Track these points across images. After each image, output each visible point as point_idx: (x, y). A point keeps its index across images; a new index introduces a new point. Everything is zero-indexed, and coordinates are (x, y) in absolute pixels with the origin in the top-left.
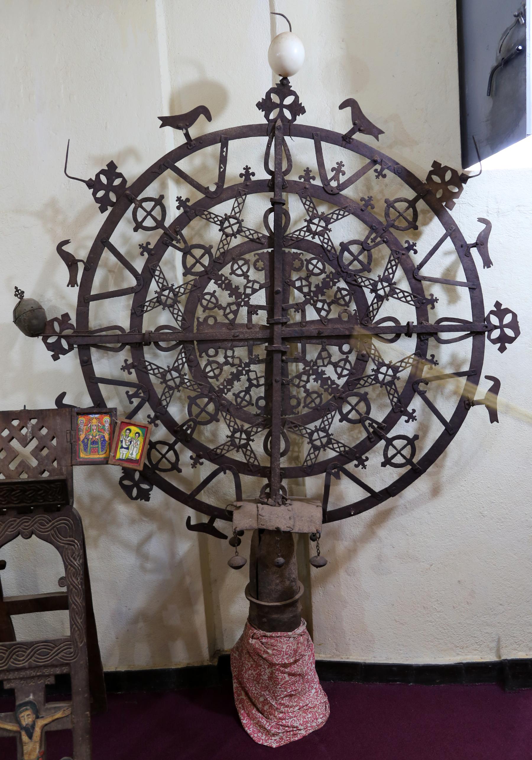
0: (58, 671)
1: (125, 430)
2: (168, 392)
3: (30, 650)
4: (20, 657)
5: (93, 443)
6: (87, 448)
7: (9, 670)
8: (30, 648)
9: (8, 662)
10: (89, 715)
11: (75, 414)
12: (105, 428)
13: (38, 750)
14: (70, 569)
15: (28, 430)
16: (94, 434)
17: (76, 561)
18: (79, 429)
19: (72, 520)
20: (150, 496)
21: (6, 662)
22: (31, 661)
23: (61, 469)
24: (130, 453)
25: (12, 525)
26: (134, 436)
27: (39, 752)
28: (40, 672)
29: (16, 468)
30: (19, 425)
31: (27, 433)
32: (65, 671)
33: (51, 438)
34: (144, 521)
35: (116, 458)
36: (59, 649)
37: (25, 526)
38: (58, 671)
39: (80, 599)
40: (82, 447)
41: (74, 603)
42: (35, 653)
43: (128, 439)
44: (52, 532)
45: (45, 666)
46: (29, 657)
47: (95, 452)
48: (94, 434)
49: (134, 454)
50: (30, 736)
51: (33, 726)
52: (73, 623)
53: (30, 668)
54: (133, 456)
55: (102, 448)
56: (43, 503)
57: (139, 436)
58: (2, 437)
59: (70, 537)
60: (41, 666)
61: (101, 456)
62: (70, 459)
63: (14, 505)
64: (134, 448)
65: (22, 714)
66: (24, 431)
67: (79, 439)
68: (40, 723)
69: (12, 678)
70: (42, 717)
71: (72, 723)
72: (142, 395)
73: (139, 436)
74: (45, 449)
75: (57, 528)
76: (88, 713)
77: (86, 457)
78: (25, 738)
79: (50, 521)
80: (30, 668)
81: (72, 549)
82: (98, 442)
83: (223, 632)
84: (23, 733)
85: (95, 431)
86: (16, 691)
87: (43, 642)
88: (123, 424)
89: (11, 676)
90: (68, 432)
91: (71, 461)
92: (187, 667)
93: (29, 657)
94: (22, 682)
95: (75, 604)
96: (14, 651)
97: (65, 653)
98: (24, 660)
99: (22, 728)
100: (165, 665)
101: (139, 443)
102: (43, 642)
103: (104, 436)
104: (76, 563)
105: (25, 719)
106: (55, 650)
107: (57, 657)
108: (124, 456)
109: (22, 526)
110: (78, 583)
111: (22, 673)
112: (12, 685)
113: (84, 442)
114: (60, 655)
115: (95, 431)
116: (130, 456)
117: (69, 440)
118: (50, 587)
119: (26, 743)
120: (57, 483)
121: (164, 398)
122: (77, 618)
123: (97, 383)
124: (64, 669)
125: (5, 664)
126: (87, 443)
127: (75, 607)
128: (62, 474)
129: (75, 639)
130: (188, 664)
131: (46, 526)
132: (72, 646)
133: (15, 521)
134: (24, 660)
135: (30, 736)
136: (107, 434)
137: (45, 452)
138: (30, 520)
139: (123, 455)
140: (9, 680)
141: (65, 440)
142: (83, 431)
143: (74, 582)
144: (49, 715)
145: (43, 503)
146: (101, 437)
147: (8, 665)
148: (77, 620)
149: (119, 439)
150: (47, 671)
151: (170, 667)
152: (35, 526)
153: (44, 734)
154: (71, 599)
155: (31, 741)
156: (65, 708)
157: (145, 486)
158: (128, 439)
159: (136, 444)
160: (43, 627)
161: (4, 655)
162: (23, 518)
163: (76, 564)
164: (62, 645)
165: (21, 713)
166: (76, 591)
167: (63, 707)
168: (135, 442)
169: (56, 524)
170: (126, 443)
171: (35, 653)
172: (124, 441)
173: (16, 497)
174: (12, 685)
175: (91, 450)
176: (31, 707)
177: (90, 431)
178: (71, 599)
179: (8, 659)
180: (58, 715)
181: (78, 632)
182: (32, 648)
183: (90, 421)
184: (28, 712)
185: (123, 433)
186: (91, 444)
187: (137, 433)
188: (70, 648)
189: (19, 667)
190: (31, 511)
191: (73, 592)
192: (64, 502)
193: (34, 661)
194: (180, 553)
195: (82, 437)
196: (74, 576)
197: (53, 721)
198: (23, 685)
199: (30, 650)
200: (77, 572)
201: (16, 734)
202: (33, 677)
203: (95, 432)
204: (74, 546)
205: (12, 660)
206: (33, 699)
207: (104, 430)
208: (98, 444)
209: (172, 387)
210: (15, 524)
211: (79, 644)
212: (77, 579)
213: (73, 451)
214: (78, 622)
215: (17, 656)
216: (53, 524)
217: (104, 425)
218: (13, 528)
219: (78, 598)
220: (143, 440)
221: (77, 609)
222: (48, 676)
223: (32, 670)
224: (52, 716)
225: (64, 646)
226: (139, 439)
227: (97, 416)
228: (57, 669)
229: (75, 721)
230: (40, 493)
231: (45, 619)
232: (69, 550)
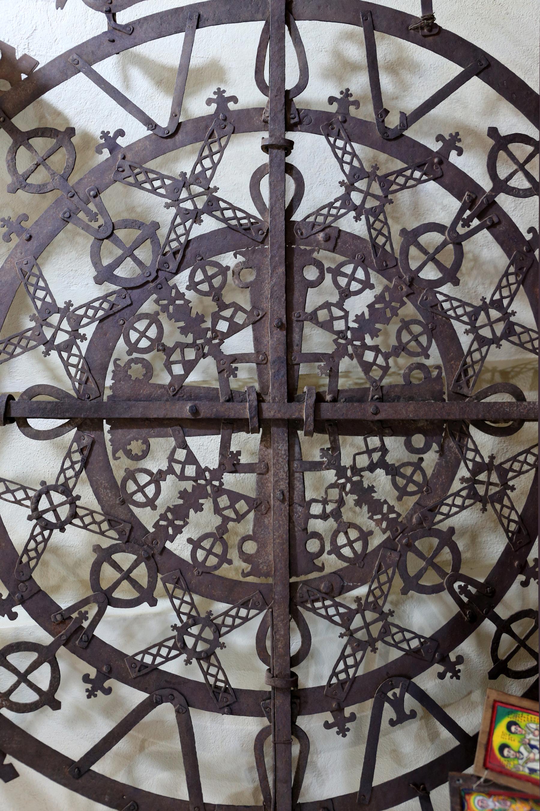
1: (502, 759)
26: (517, 738)
43: (525, 754)
72: (397, 691)
158: (525, 754)
168: (531, 736)
185: (510, 765)
209: (383, 627)
220: (525, 715)
226: (522, 724)
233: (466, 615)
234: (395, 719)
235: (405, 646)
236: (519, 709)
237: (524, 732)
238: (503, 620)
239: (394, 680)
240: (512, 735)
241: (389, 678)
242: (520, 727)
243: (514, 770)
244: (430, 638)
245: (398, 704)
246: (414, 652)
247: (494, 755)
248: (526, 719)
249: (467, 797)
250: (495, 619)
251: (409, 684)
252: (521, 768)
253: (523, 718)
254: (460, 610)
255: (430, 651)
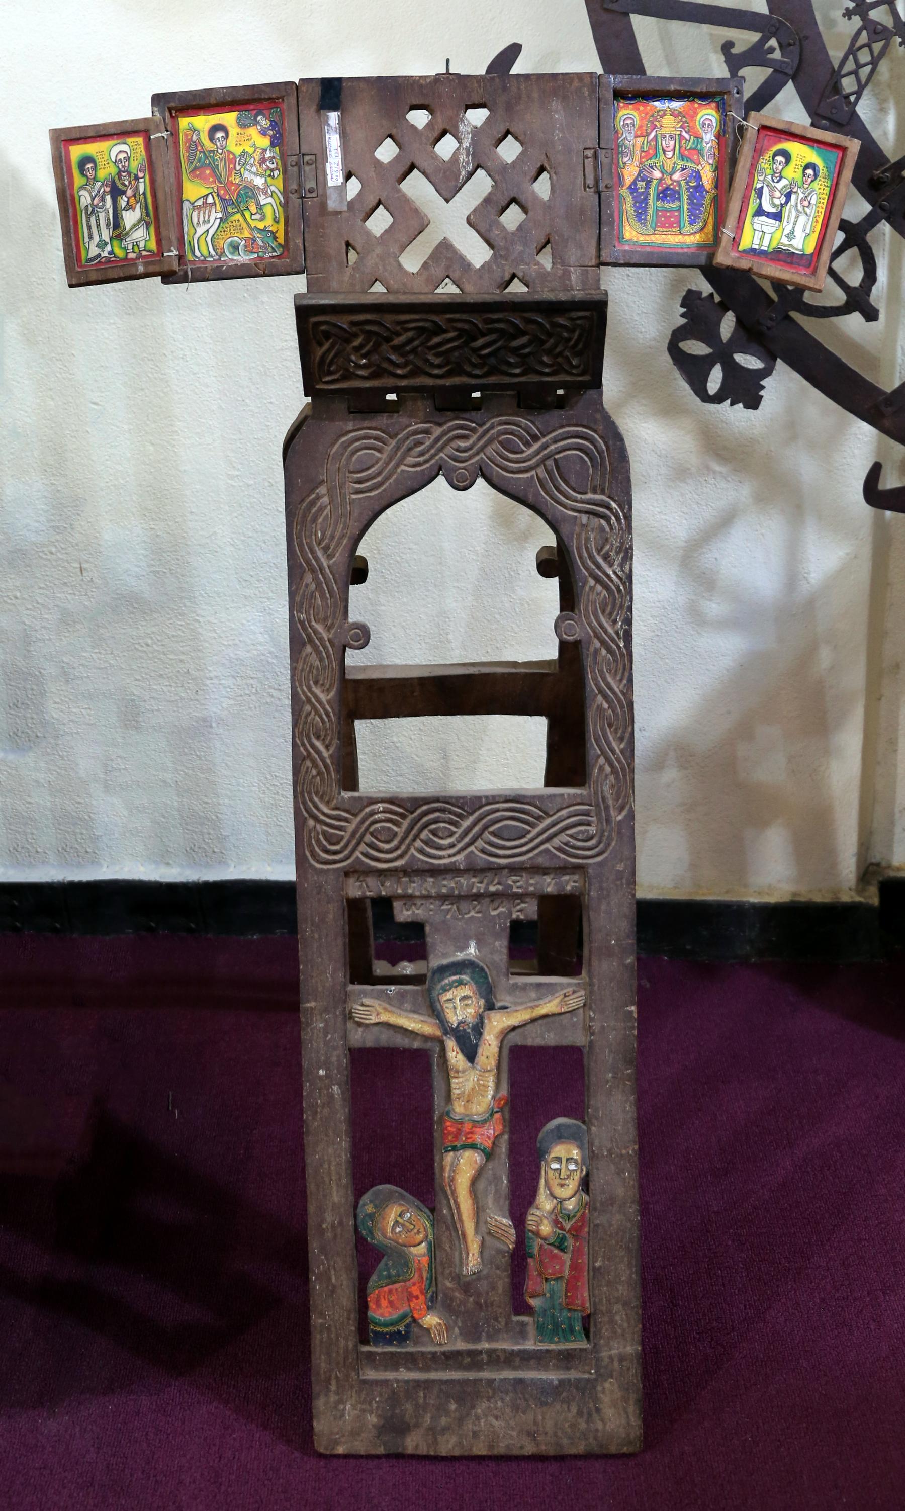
0: (549, 885)
1: (771, 153)
2: (868, 45)
3: (471, 819)
4: (442, 838)
5: (665, 196)
6: (645, 210)
7: (410, 872)
8: (472, 814)
9: (408, 849)
10: (635, 1015)
11: (611, 95)
12: (702, 149)
13: (491, 1093)
14: (592, 589)
15: (460, 143)
16: (669, 166)
17: (611, 565)
18: (618, 146)
19: (601, 437)
20: (762, 393)
21: (403, 847)
22: (472, 852)
23: (566, 274)
24: (787, 232)
25: (419, 443)
26: (798, 176)
27: (494, 1097)
28: (499, 884)
29: (425, 265)
30: (429, 125)
31: (457, 152)
32: (569, 888)
33: (534, 172)
34: (714, 472)
35: (741, 248)
36: (554, 825)
37: (457, 450)
38: (549, 885)
39: (621, 680)
40: (628, 206)
41: (601, 692)
42: (486, 827)
43: (780, 185)
44: (541, 471)
45: (514, 870)
46: (467, 840)
47: (671, 226)
48: (669, 166)
49: (799, 234)
50: (471, 1055)
51: (478, 1028)
52: (599, 752)
53: (473, 870)
54: (793, 242)
55: (691, 213)
56: (523, 379)
57: (816, 176)
58: (378, 163)
59: (594, 491)
60: (501, 868)
61: (690, 240)
62: (594, 243)
63: (429, 382)
64: (797, 217)
65: (449, 995)
66: (446, 147)
67: (620, 179)
68: (497, 1023)
69: (417, 893)
70: (505, 1008)
71: (589, 1030)
72: (777, 55)
73: (816, 176)
74: (514, 209)
75: (555, 460)
76: (633, 1008)
77: (642, 239)
78: (455, 1057)
79: (535, 438)
80: (473, 870)
81: (602, 529)
82: (679, 193)
83: (897, 815)
84: (451, 1044)
85: (670, 154)
86: (427, 929)
87: (383, 801)
88: (765, 132)
89: (414, 887)
90: (589, 153)
91: (599, 250)
92: (792, 902)
93: (467, 840)
94: (444, 907)
95: (605, 697)
96: (425, 819)
97: (571, 836)
98: (452, 846)
99: (447, 1029)
100: (727, 892)
101: (813, 201)
102: (507, 801)
103: (698, 172)
104: (611, 573)
105: (455, 1008)
106: (542, 826)
107: (547, 846)
108: (766, 243)
109: (449, 450)
110: (617, 633)
111: (445, 883)
112: (417, 912)
113: (636, 190)
114: (556, 841)
115: (670, 154)
116: (785, 240)
117: (590, 181)
118: (417, 652)
119: (457, 1072)
120: (575, 314)
121: (850, 65)
122: (611, 738)
123: (627, 14)
124: (567, 882)
125: (399, 852)
126: (647, 194)
127: (606, 706)
128: (567, 288)
129: (604, 798)
130: (795, 894)
131: (522, 452)
132: (594, 819)
133: (427, 432)
134: (452, 846)
135: (471, 1055)
136: (708, 168)
137: (512, 217)
138: (473, 430)
139: (762, 239)
140: (408, 898)
141: (580, 180)
142: (632, 154)
143: (606, 632)
144: (522, 1003)
145: (523, 379)
146: (691, 176)
147: (407, 858)
148: (609, 744)
149: (749, 185)
150: (517, 884)
151: (745, 899)
152: (489, 450)
153: (506, 1052)
154: (595, 679)
155: (473, 1068)
156: (570, 989)
157: (750, 362)
158: (780, 185)
159: (806, 203)
160: (390, 762)
161: (395, 828)
162: (451, 424)
163: (613, 576)
164: (564, 813)
165: (445, 990)
166: (609, 656)
167: (562, 986)
168: (801, 196)
169: (553, 447)
170: (772, 197)
171: (486, 827)
172: (766, 191)
173: (437, 355)
174: (417, 912)
175: (657, 214)
176: (472, 979)
177: (656, 155)
178: (595, 679)
179: (407, 842)
180: (550, 1006)
181: (612, 778)
182: (477, 814)
183: (653, 122)
184: (466, 991)
185: (764, 164)
186: (658, 198)
187: (810, 166)
188: (589, 824)
189: (440, 865)
190: (476, 406)
191: (599, 659)
192: (586, 378)
193: (483, 851)
194: (813, 575)
195: (630, 173)
196: (603, 612)
197: (534, 1020)
198: (449, 917)
199: (471, 819)
200: (615, 599)
201: (429, 1045)
202: (477, 897)
203: (670, 160)
204: (607, 519)
205: (418, 844)
206: (476, 957)
207: (700, 153)
208: (679, 199)
209: (885, 28)
210: (428, 443)
211: (613, 813)
212: (615, 622)
213: (604, 218)
214: (613, 751)
215: (434, 833)
216: (545, 446)
217: (698, 138)
218: (422, 454)
219: (614, 678)
220: (827, 190)
221: (610, 711)
222: (521, 897)
223: (474, 877)
224: (532, 1008)
225: (569, 817)
226: (816, 185)
227: (676, 105)
228: (548, 879)
229: (596, 1026)
230: (515, 343)
231: (395, 739)
232: (593, 530)
233: (883, 172)
234: (734, 51)
235: (850, 65)
236: (835, 182)
237: (806, 186)
238: (866, 234)
239: (796, 49)
240: (801, 169)
241: (800, 40)
242: (812, 181)
243: (759, 168)
244: (854, 112)
245: (756, 56)
246: (836, 83)
247: (775, 143)
248: (821, 191)
249: (713, 105)
250: (870, 221)
251: (786, 74)
252: (761, 178)
253: (822, 187)
254: (893, 161)
255: (834, 111)
